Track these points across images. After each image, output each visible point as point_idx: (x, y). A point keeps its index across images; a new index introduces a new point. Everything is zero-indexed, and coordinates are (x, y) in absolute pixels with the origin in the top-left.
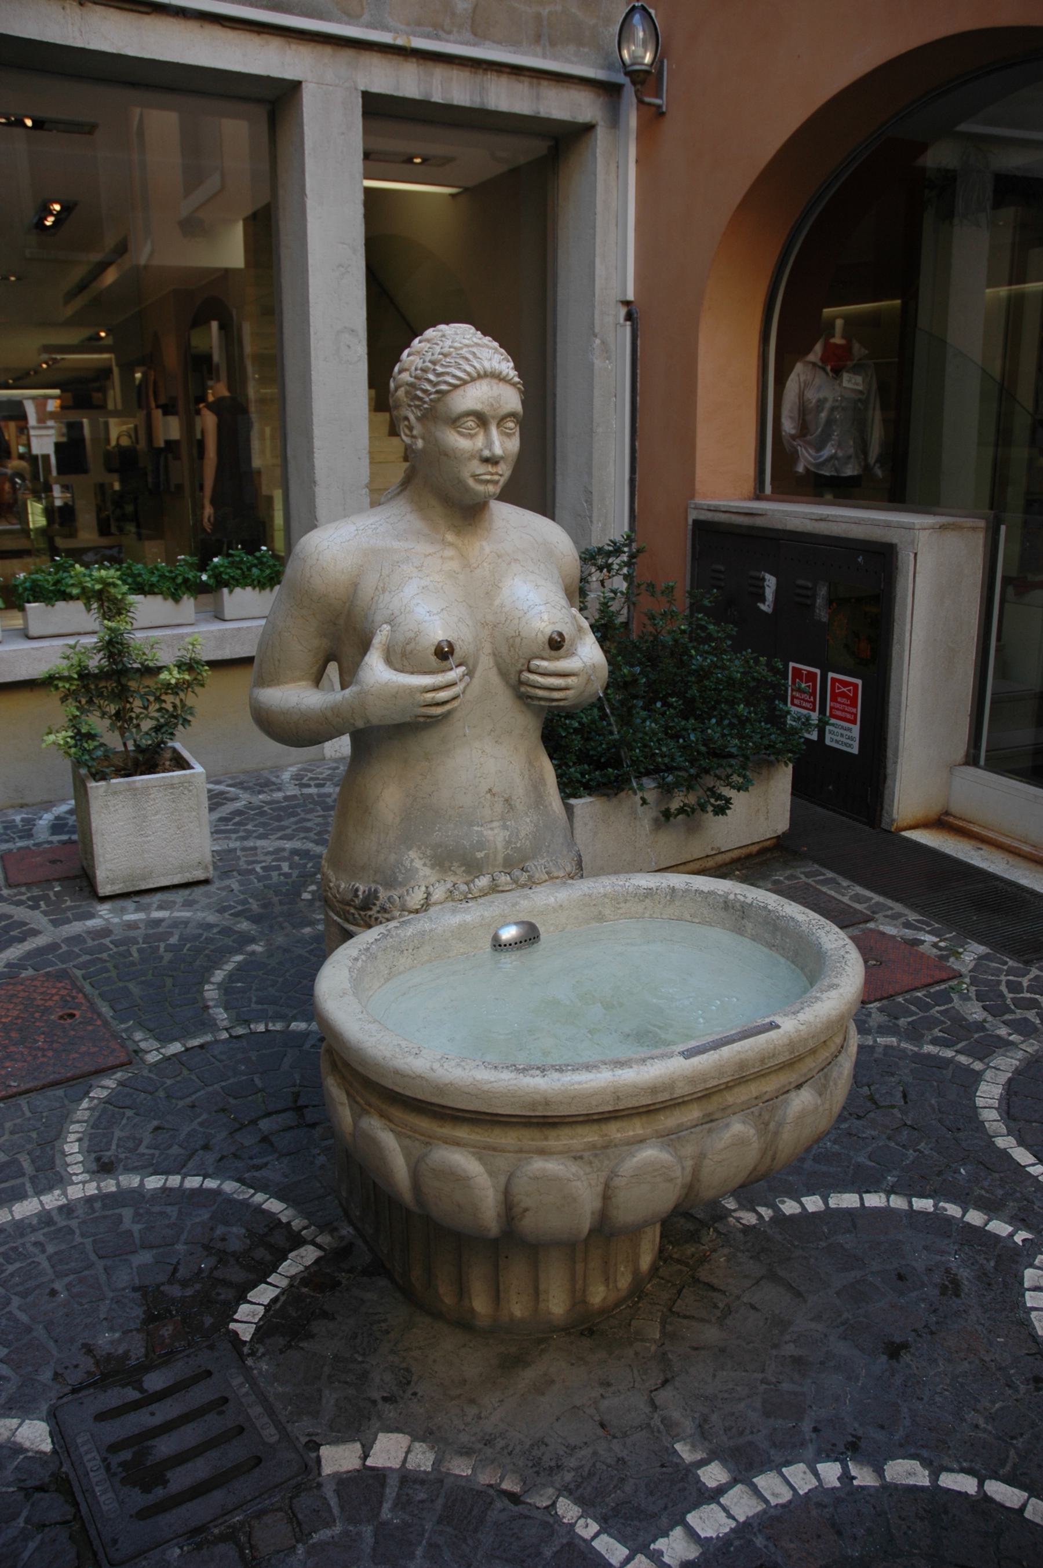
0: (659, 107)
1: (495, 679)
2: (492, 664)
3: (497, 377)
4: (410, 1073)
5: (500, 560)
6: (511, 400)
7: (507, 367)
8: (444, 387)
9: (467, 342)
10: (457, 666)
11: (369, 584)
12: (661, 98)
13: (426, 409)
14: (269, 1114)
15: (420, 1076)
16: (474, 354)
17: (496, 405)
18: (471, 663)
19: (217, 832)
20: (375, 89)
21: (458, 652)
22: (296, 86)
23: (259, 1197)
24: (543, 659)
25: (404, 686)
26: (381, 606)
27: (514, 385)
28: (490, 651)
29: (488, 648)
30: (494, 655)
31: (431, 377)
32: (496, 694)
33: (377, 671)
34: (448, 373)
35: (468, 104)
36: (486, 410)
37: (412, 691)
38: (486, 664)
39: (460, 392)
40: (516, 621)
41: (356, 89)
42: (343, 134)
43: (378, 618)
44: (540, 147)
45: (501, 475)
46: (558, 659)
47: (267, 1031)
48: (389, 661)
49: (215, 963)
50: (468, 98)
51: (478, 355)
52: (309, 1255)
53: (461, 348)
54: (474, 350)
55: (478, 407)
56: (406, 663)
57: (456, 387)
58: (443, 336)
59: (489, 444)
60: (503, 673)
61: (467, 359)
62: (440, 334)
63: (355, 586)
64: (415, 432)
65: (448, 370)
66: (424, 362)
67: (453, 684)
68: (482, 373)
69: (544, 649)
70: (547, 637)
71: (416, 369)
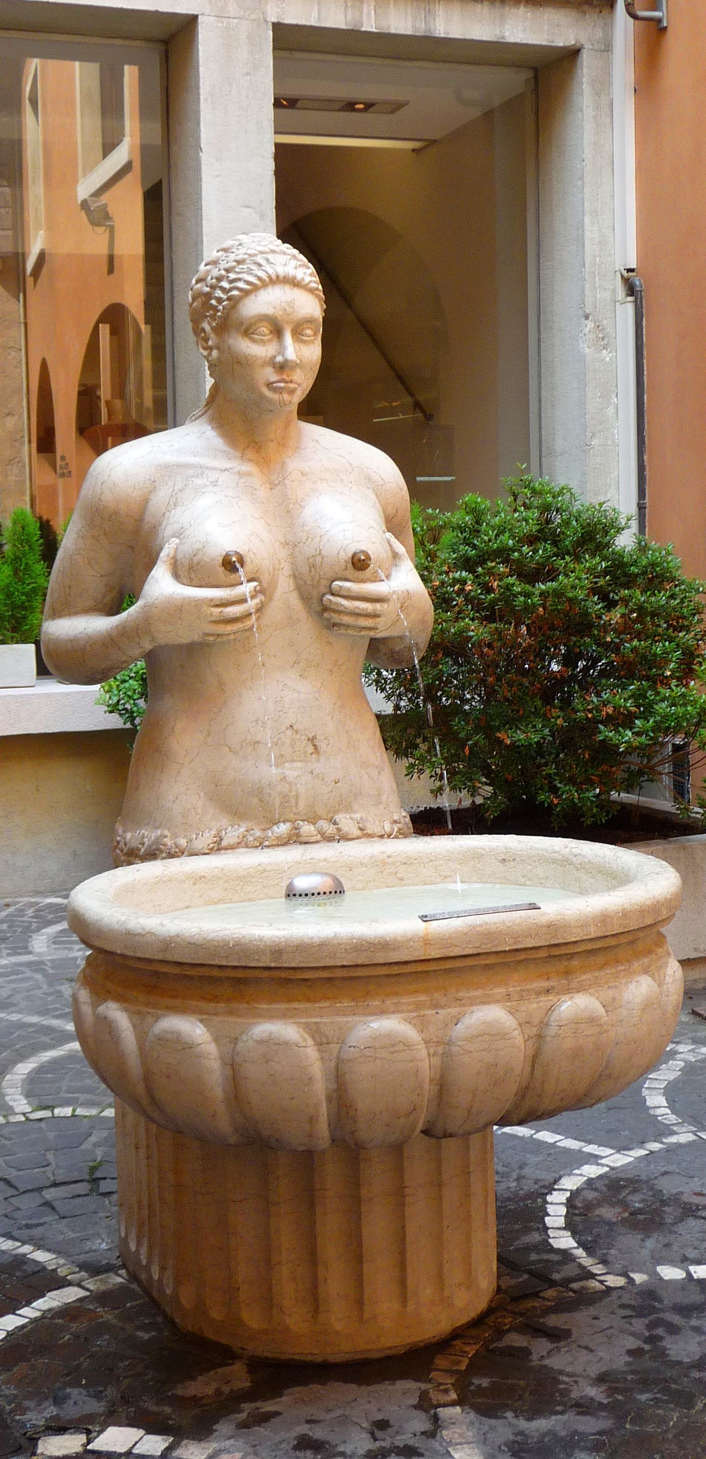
0: (659, 21)
1: (294, 599)
2: (292, 587)
3: (294, 283)
4: (140, 931)
5: (305, 478)
6: (311, 306)
7: (307, 272)
8: (235, 293)
9: (261, 249)
10: (249, 581)
11: (159, 500)
12: (661, 10)
13: (220, 317)
14: (55, 1185)
15: (149, 933)
16: (267, 260)
17: (289, 310)
18: (265, 578)
19: (55, 943)
20: (288, 20)
21: (249, 566)
22: (190, 23)
23: (26, 1249)
24: (346, 580)
25: (189, 598)
26: (172, 521)
27: (312, 291)
28: (290, 573)
29: (286, 570)
30: (295, 577)
31: (225, 284)
32: (298, 620)
33: (162, 585)
34: (240, 280)
35: (409, 33)
36: (279, 314)
37: (198, 604)
38: (285, 587)
39: (252, 297)
40: (317, 540)
41: (266, 21)
42: (248, 74)
43: (168, 532)
44: (514, 82)
45: (299, 385)
46: (363, 581)
47: (73, 1116)
48: (176, 576)
49: (22, 1057)
50: (410, 25)
51: (272, 260)
52: (71, 1295)
53: (255, 255)
54: (270, 256)
55: (270, 311)
56: (193, 576)
57: (246, 293)
58: (240, 245)
59: (282, 350)
60: (305, 598)
61: (260, 265)
62: (237, 243)
63: (146, 502)
64: (210, 343)
65: (241, 276)
66: (219, 270)
67: (243, 601)
68: (274, 277)
69: (346, 569)
70: (350, 554)
71: (212, 279)
